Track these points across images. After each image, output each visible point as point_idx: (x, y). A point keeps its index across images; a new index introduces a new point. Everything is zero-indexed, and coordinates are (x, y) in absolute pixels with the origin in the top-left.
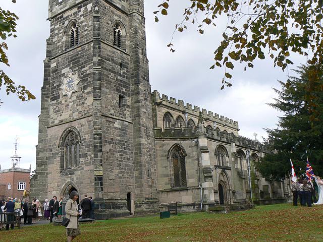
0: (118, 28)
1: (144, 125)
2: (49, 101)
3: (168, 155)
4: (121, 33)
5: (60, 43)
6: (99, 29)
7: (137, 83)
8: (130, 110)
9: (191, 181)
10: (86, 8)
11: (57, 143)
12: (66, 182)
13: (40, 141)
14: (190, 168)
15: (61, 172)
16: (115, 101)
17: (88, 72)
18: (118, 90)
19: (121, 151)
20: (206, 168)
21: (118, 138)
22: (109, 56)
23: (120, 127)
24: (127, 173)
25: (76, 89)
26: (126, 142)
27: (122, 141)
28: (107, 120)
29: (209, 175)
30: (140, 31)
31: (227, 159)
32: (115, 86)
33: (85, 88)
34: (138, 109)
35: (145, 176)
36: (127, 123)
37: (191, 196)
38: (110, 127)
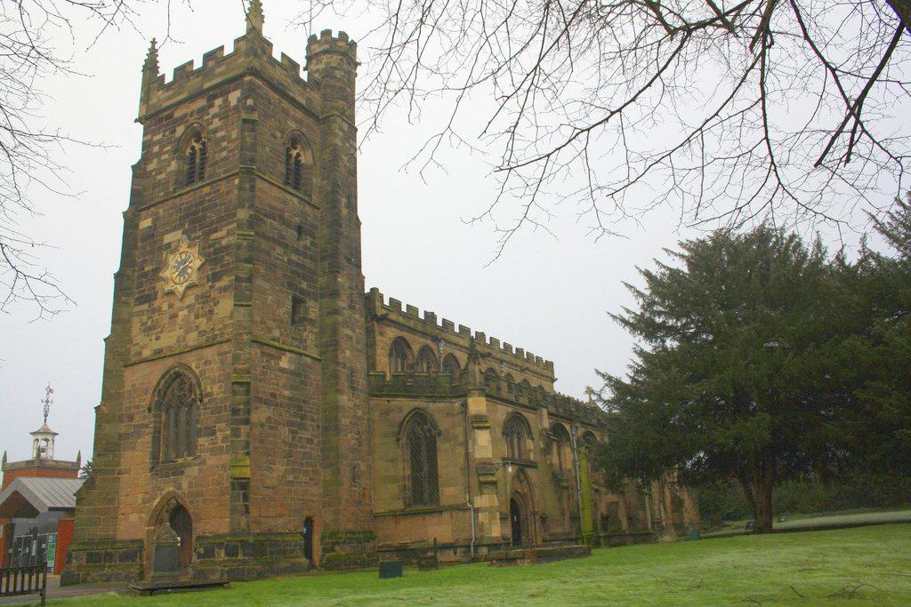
4: (303, 159)
5: (163, 176)
6: (253, 148)
8: (316, 330)
9: (450, 493)
10: (226, 101)
12: (164, 492)
13: (107, 394)
14: (448, 463)
17: (224, 242)
18: (291, 285)
20: (484, 463)
21: (287, 393)
24: (306, 473)
25: (194, 278)
27: (297, 400)
28: (263, 353)
31: (530, 444)
33: (216, 277)
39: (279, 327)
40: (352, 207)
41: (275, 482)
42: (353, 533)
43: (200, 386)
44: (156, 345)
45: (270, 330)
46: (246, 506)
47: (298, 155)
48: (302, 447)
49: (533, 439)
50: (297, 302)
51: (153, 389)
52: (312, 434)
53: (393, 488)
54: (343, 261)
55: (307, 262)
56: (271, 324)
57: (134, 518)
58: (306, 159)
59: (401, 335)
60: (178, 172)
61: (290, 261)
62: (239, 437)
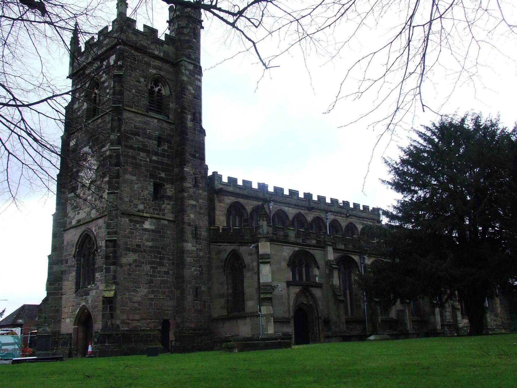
0: (158, 86)
1: (192, 223)
2: (67, 193)
3: (225, 266)
4: (163, 92)
6: (121, 93)
7: (182, 164)
8: (171, 203)
9: (250, 305)
10: (109, 62)
11: (73, 253)
12: (81, 305)
13: (54, 248)
15: (76, 291)
16: (146, 192)
18: (152, 176)
19: (154, 262)
20: (266, 286)
21: (150, 244)
22: (138, 128)
23: (153, 227)
24: (164, 293)
26: (163, 248)
27: (156, 247)
28: (131, 221)
29: (268, 296)
30: (190, 88)
31: (316, 272)
32: (147, 171)
34: (182, 200)
35: (190, 298)
36: (166, 222)
37: (250, 327)
38: (136, 229)
39: (143, 203)
40: (197, 118)
41: (139, 299)
42: (195, 330)
43: (96, 242)
44: (78, 217)
45: (136, 206)
46: (112, 314)
47: (160, 90)
48: (159, 277)
49: (318, 268)
50: (158, 187)
51: (76, 243)
52: (168, 269)
53: (222, 301)
54: (188, 156)
55: (165, 160)
56: (136, 202)
57: (68, 320)
58: (165, 92)
59: (237, 200)
60: (87, 109)
61: (151, 161)
62: (110, 273)
